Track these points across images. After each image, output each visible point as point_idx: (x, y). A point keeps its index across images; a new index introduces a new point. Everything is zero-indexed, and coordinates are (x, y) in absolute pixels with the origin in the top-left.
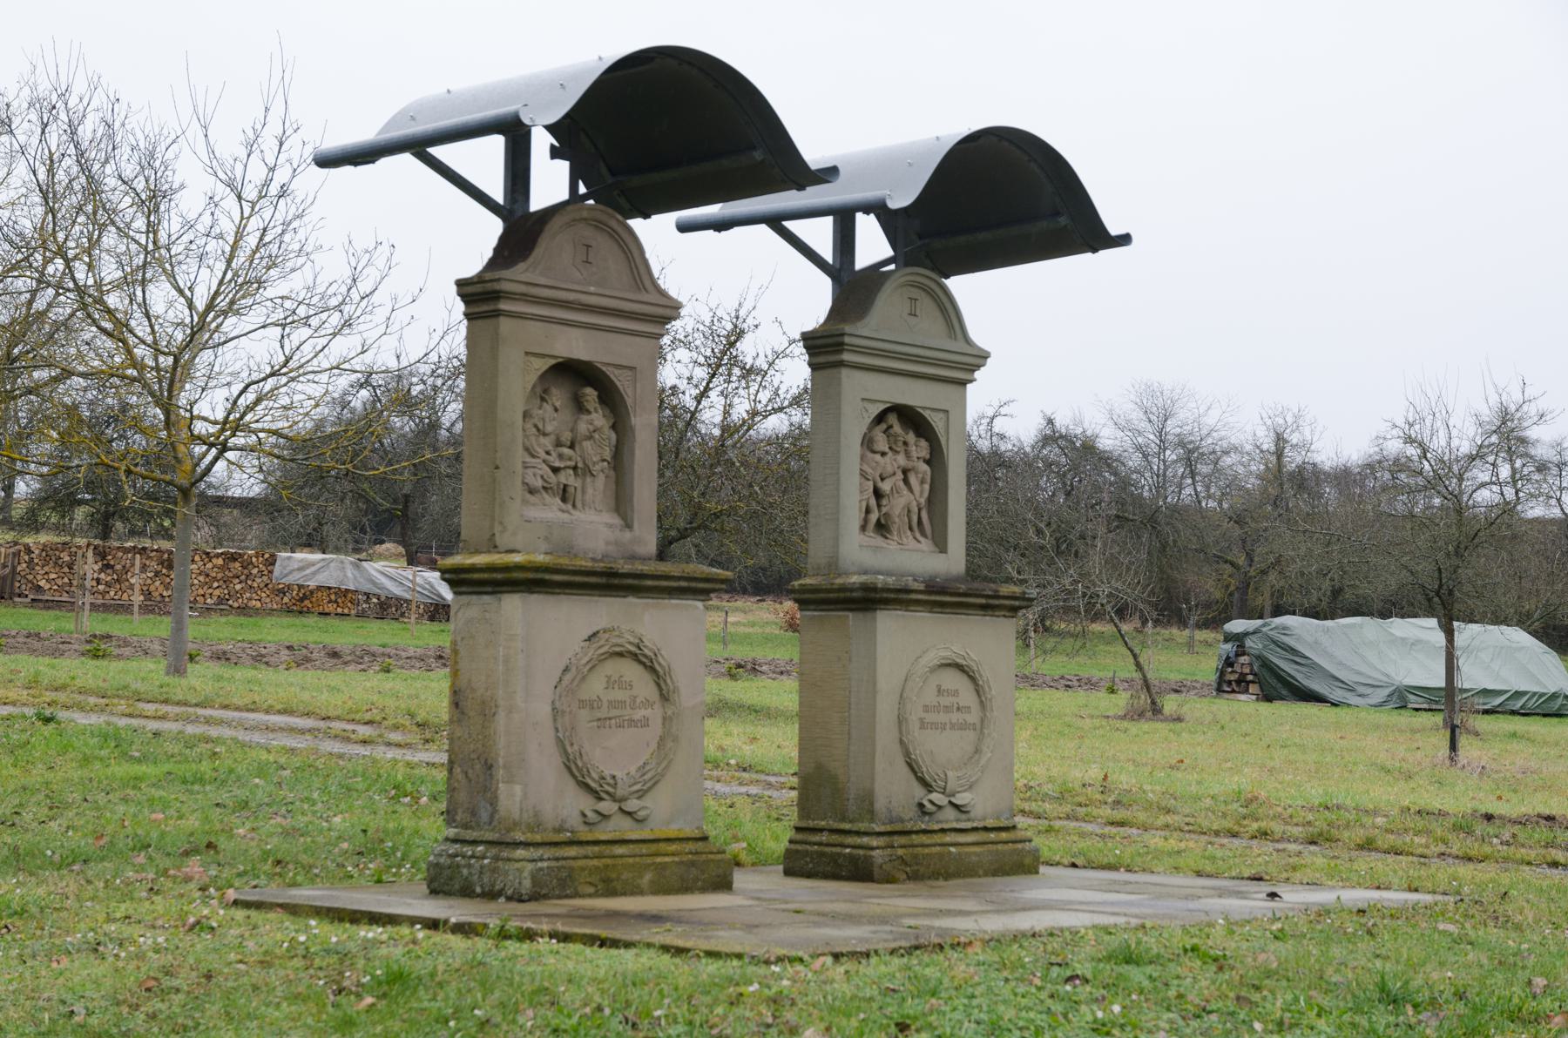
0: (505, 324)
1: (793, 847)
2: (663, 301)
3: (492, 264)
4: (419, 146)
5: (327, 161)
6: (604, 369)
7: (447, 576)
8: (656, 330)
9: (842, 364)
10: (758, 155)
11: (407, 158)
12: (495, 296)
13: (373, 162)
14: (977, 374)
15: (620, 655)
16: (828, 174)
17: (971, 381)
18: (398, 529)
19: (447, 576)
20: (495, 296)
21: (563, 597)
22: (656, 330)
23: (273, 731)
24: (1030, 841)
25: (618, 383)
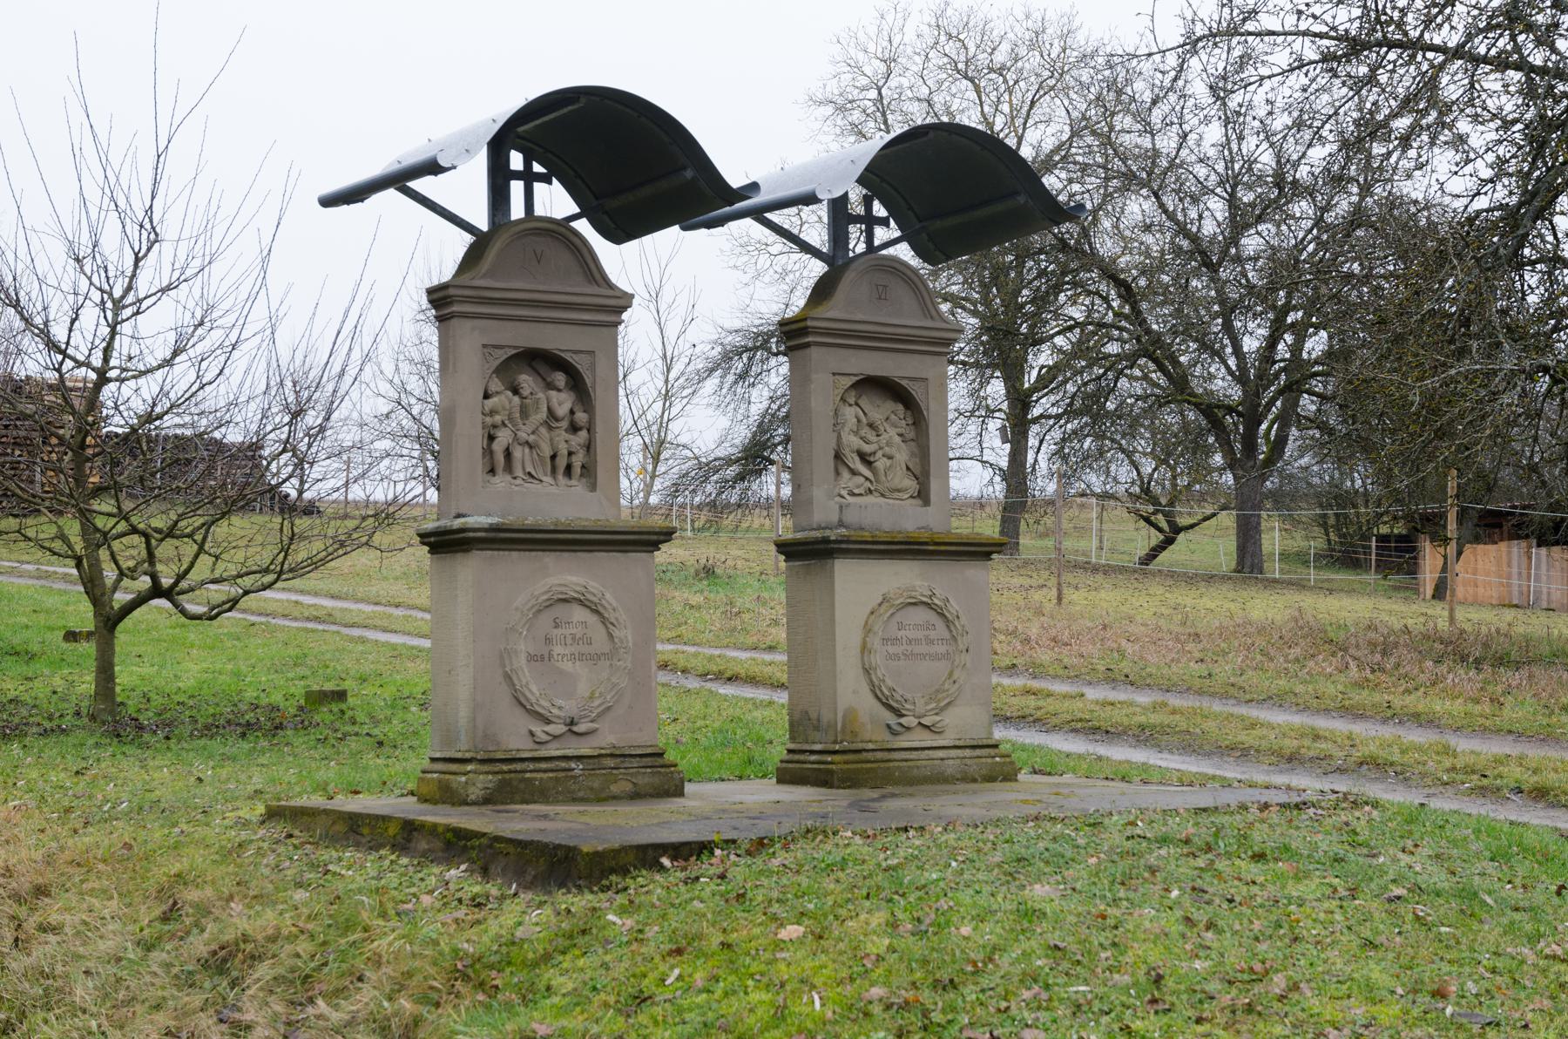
0: (814, 352)
1: (784, 765)
2: (610, 293)
3: (454, 276)
4: (399, 180)
5: (329, 201)
6: (562, 355)
7: (426, 540)
8: (612, 318)
9: (808, 345)
10: (689, 174)
11: (391, 194)
12: (804, 332)
13: (362, 201)
14: (625, 316)
15: (565, 600)
16: (754, 187)
17: (620, 323)
18: (113, 492)
19: (426, 540)
20: (804, 332)
21: (566, 555)
22: (612, 318)
23: (1501, 661)
24: (675, 766)
25: (579, 367)
